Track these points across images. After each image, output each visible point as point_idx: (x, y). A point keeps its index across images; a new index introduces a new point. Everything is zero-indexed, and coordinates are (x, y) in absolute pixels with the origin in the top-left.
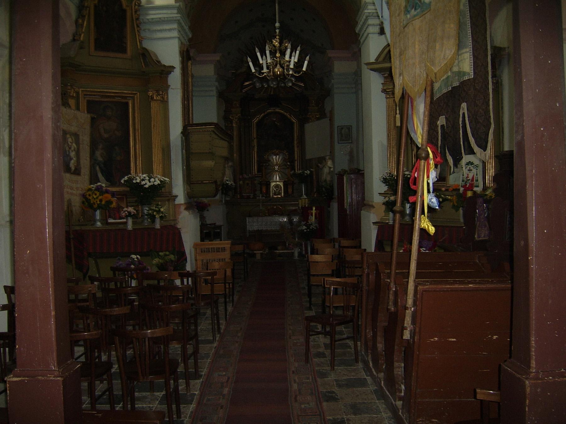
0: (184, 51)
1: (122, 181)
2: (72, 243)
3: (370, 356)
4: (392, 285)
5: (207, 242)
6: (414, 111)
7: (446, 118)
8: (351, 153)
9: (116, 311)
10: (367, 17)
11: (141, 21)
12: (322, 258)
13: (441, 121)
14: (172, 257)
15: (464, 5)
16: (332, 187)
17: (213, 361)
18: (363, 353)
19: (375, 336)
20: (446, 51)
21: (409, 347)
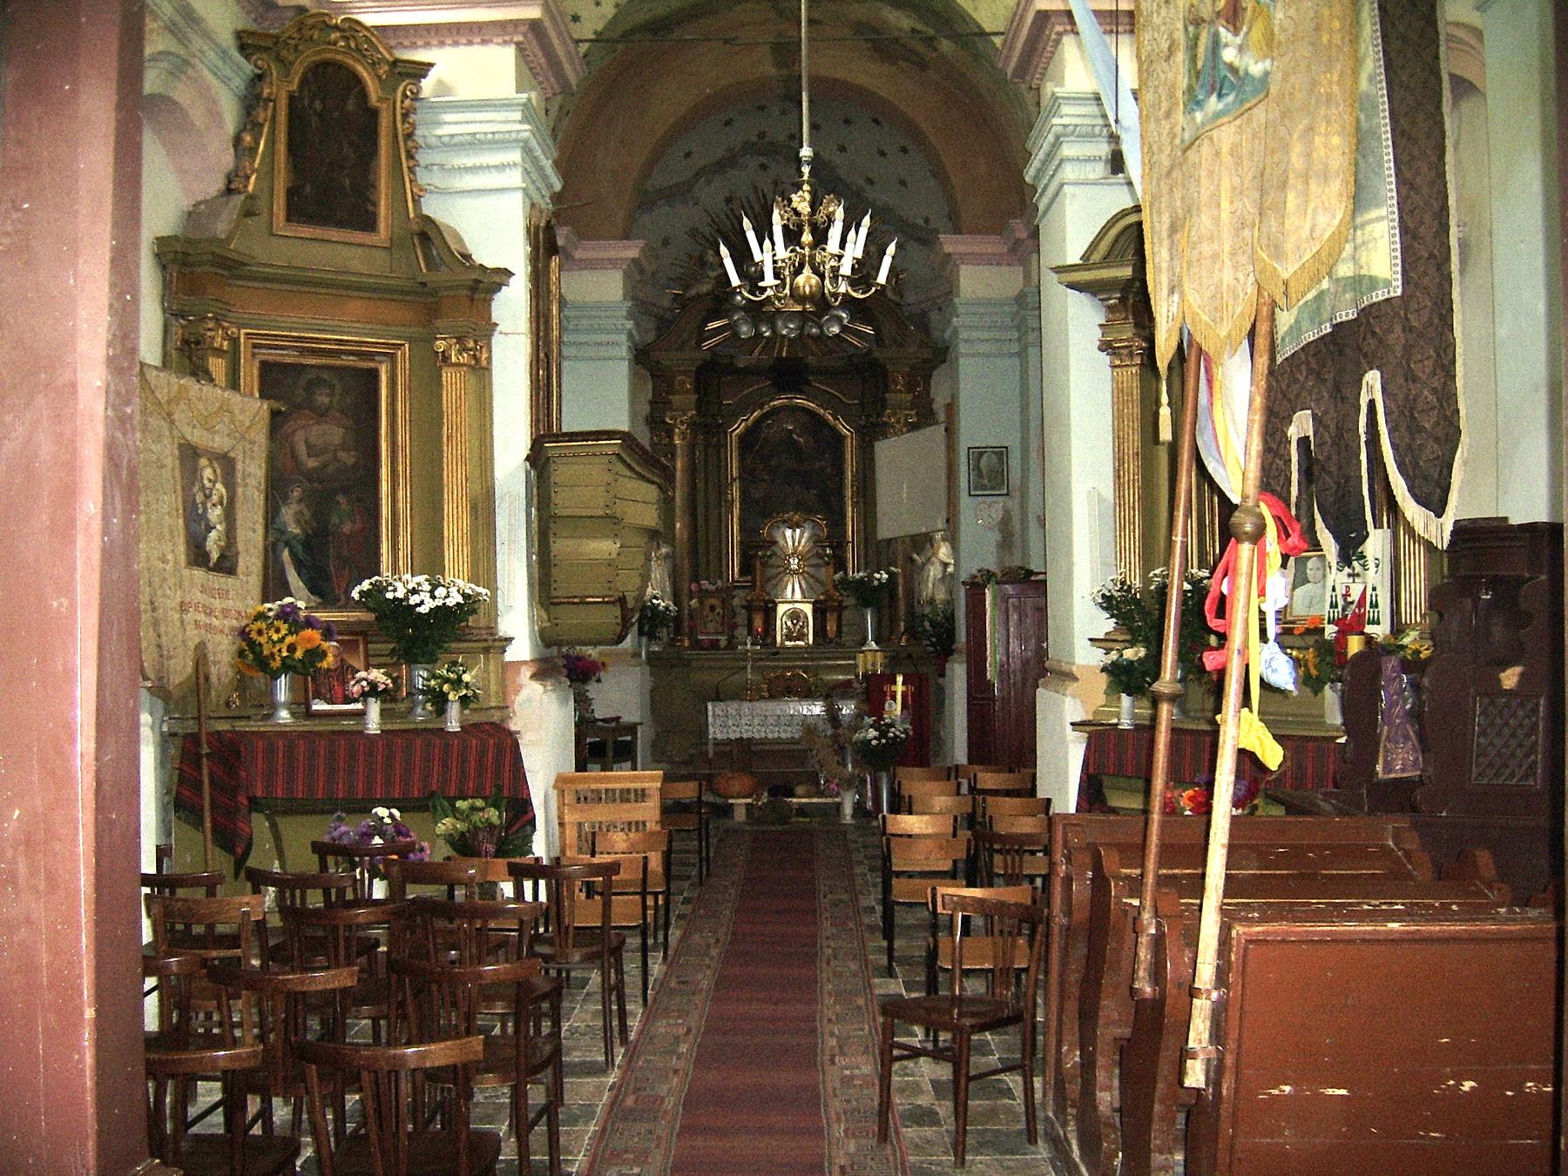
0: (537, 228)
1: (355, 594)
2: (205, 772)
3: (1072, 1126)
4: (1146, 916)
5: (594, 772)
6: (1217, 395)
7: (1314, 416)
8: (1005, 524)
9: (323, 979)
10: (1057, 138)
11: (420, 141)
12: (921, 826)
13: (1301, 425)
14: (493, 815)
15: (1371, 79)
16: (950, 619)
17: (604, 1130)
18: (1050, 1114)
19: (1088, 1065)
20: (1314, 214)
21: (1199, 1108)
